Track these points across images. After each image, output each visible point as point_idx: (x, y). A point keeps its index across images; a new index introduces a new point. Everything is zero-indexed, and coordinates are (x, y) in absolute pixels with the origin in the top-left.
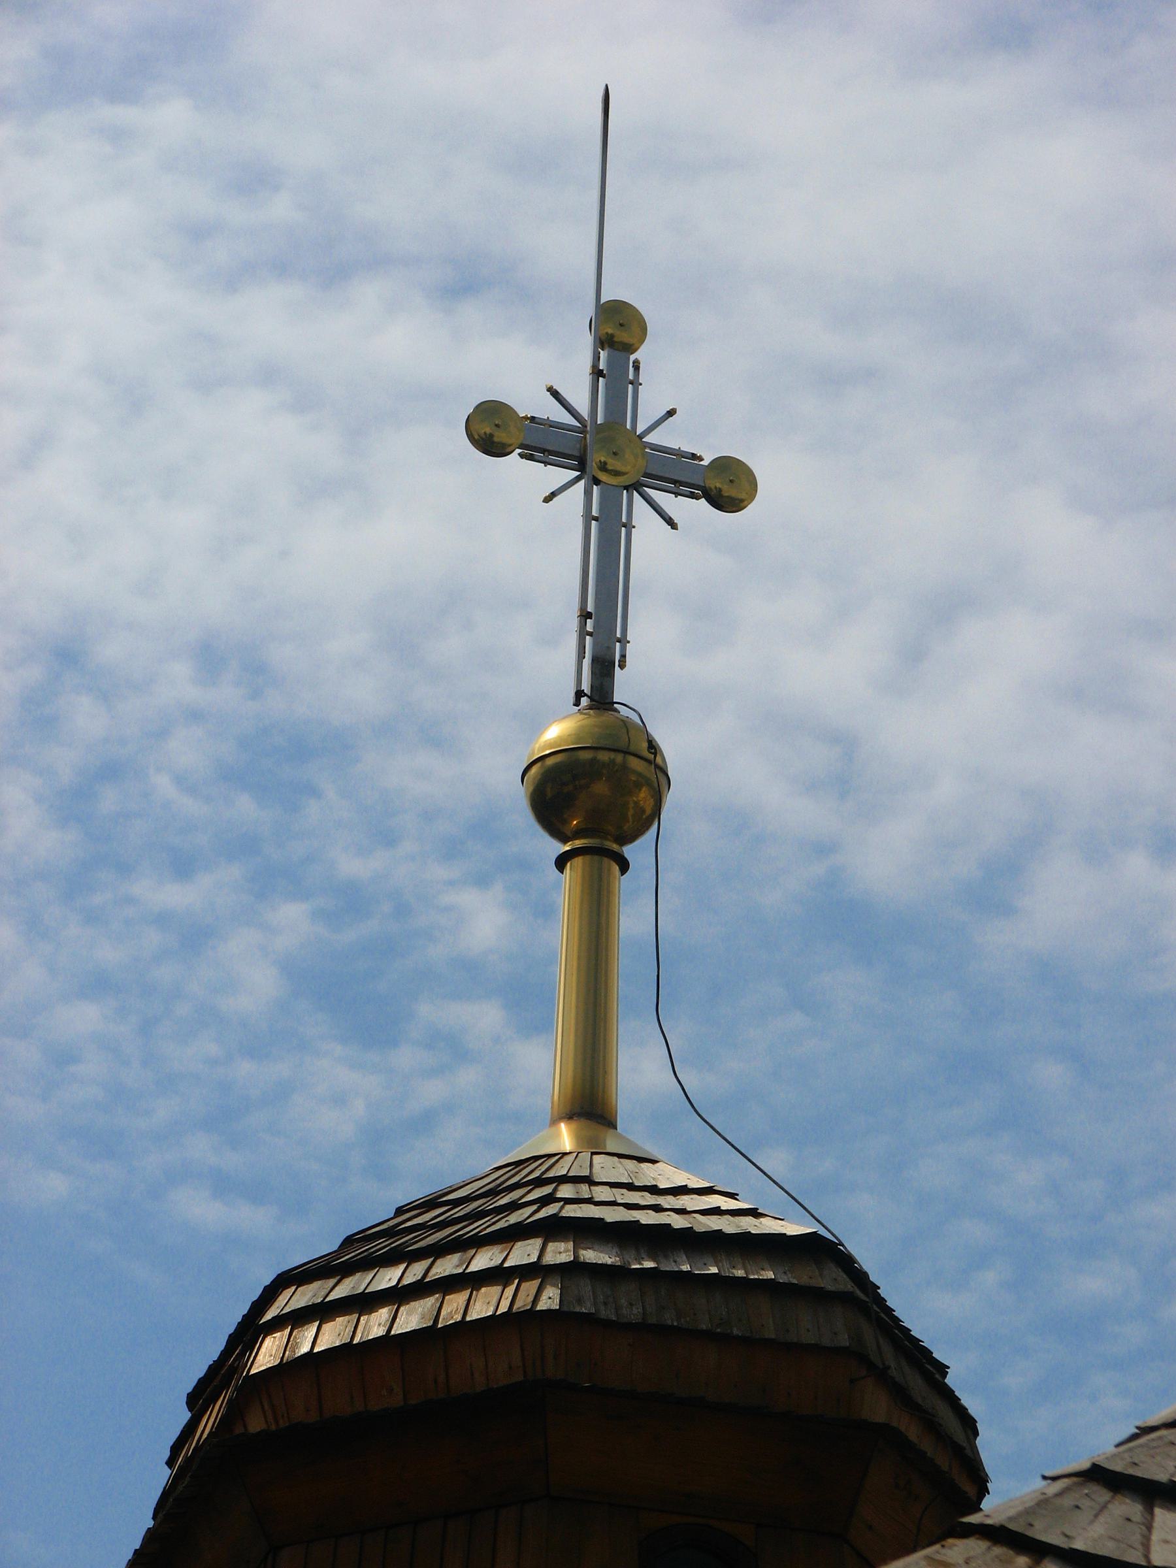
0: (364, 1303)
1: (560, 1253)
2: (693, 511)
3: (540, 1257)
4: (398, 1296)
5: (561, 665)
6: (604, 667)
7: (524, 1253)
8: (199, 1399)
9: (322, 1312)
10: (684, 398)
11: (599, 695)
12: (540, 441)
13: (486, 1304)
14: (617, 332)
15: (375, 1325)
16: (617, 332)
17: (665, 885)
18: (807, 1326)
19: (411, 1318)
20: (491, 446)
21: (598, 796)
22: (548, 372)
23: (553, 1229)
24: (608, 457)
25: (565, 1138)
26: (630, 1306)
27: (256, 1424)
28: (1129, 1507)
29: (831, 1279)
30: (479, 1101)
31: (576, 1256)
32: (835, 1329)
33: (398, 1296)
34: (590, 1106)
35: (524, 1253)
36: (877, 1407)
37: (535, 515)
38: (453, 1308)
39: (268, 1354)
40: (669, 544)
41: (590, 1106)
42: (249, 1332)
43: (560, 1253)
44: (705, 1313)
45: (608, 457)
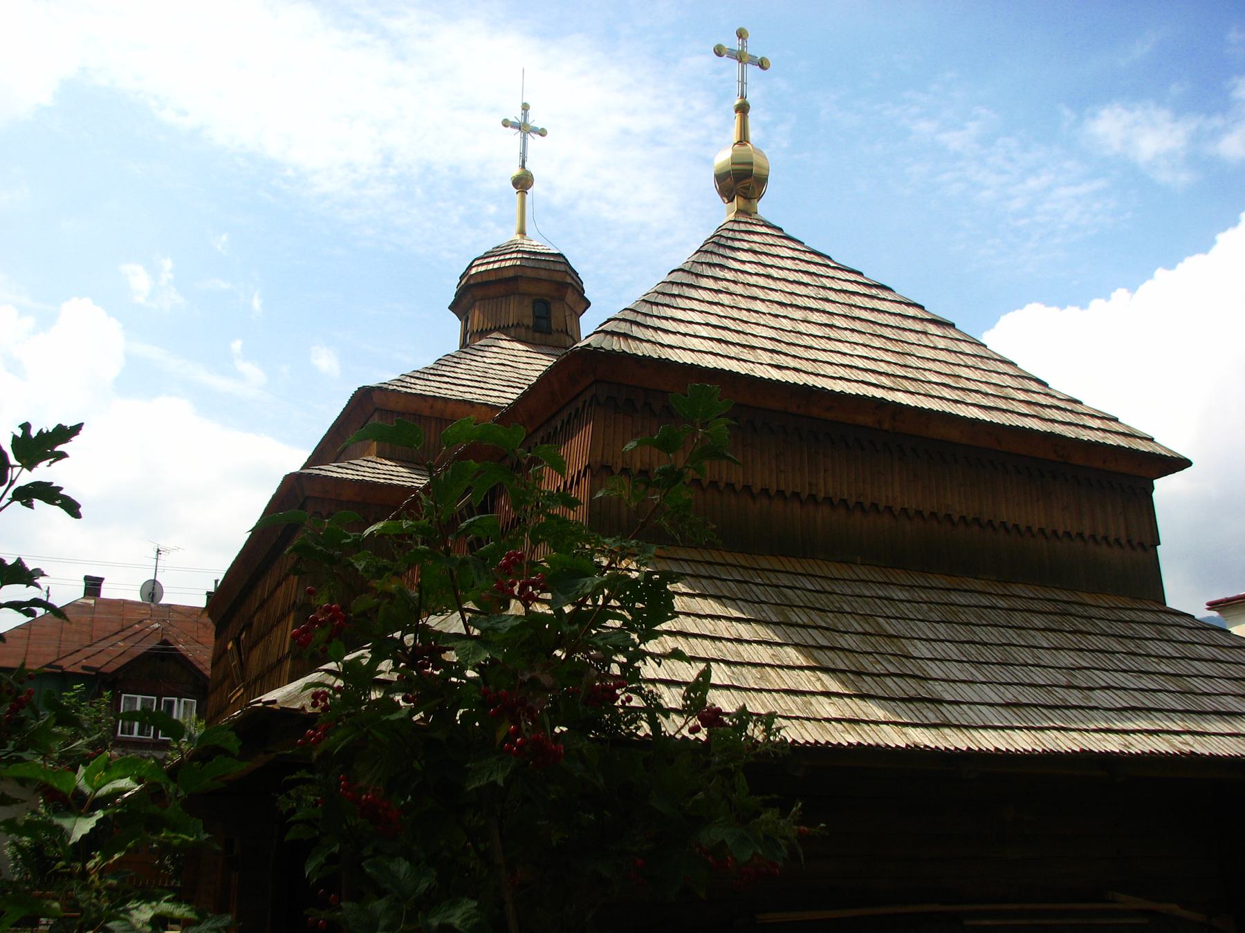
0: (488, 263)
1: (520, 255)
2: (537, 137)
3: (716, 687)
4: (494, 262)
5: (518, 162)
6: (523, 162)
7: (514, 255)
8: (461, 278)
9: (482, 264)
10: (535, 120)
11: (523, 166)
12: (514, 125)
13: (508, 263)
14: (525, 107)
15: (490, 267)
16: (525, 107)
17: (535, 190)
18: (559, 267)
19: (496, 266)
20: (505, 126)
21: (523, 183)
22: (515, 115)
23: (518, 252)
24: (523, 128)
25: (518, 237)
26: (530, 264)
27: (472, 282)
28: (648, 305)
29: (562, 260)
30: (506, 235)
31: (528, 612)
32: (562, 268)
33: (494, 262)
34: (522, 232)
35: (514, 255)
36: (569, 280)
37: (514, 136)
38: (503, 264)
39: (473, 271)
40: (534, 141)
41: (522, 232)
42: (470, 267)
43: (520, 255)
44: (543, 265)
45: (523, 128)
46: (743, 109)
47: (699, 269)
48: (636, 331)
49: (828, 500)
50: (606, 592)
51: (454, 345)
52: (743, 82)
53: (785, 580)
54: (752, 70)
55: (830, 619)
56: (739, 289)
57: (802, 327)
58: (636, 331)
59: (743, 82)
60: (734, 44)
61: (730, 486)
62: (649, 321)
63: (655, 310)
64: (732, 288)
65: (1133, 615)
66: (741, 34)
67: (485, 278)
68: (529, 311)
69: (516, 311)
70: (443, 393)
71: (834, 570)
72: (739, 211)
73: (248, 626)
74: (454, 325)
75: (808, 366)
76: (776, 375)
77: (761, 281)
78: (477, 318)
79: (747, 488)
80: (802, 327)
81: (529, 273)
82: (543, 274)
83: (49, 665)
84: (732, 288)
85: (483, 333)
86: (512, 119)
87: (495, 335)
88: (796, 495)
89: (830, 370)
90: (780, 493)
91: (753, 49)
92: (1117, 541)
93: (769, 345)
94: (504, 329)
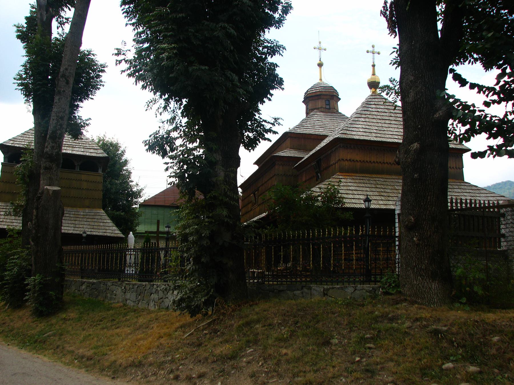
10: (323, 46)
22: (317, 45)
26: (324, 90)
30: (316, 81)
36: (335, 94)
40: (323, 52)
41: (321, 80)
44: (327, 90)
46: (374, 66)
47: (362, 112)
48: (348, 132)
49: (387, 163)
50: (492, 13)
51: (304, 116)
52: (374, 59)
53: (377, 179)
54: (376, 55)
55: (385, 187)
56: (370, 116)
57: (383, 125)
58: (348, 132)
59: (374, 59)
60: (371, 49)
61: (367, 161)
62: (351, 129)
63: (352, 126)
64: (369, 116)
65: (454, 184)
66: (373, 47)
67: (312, 95)
68: (324, 103)
69: (321, 103)
70: (305, 132)
71: (388, 177)
72: (373, 92)
73: (258, 190)
74: (303, 107)
75: (383, 136)
76: (375, 139)
77: (376, 113)
78: (310, 105)
79: (370, 161)
80: (383, 125)
81: (324, 93)
82: (327, 93)
83: (172, 204)
84: (369, 116)
85: (312, 110)
86: (316, 47)
87: (315, 111)
88: (380, 162)
89: (387, 136)
90: (377, 162)
91: (376, 50)
92: (453, 168)
93: (375, 131)
94: (317, 109)
